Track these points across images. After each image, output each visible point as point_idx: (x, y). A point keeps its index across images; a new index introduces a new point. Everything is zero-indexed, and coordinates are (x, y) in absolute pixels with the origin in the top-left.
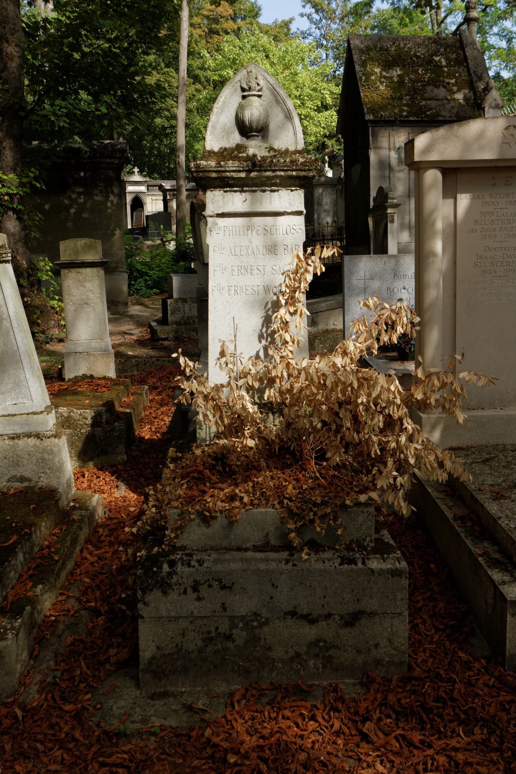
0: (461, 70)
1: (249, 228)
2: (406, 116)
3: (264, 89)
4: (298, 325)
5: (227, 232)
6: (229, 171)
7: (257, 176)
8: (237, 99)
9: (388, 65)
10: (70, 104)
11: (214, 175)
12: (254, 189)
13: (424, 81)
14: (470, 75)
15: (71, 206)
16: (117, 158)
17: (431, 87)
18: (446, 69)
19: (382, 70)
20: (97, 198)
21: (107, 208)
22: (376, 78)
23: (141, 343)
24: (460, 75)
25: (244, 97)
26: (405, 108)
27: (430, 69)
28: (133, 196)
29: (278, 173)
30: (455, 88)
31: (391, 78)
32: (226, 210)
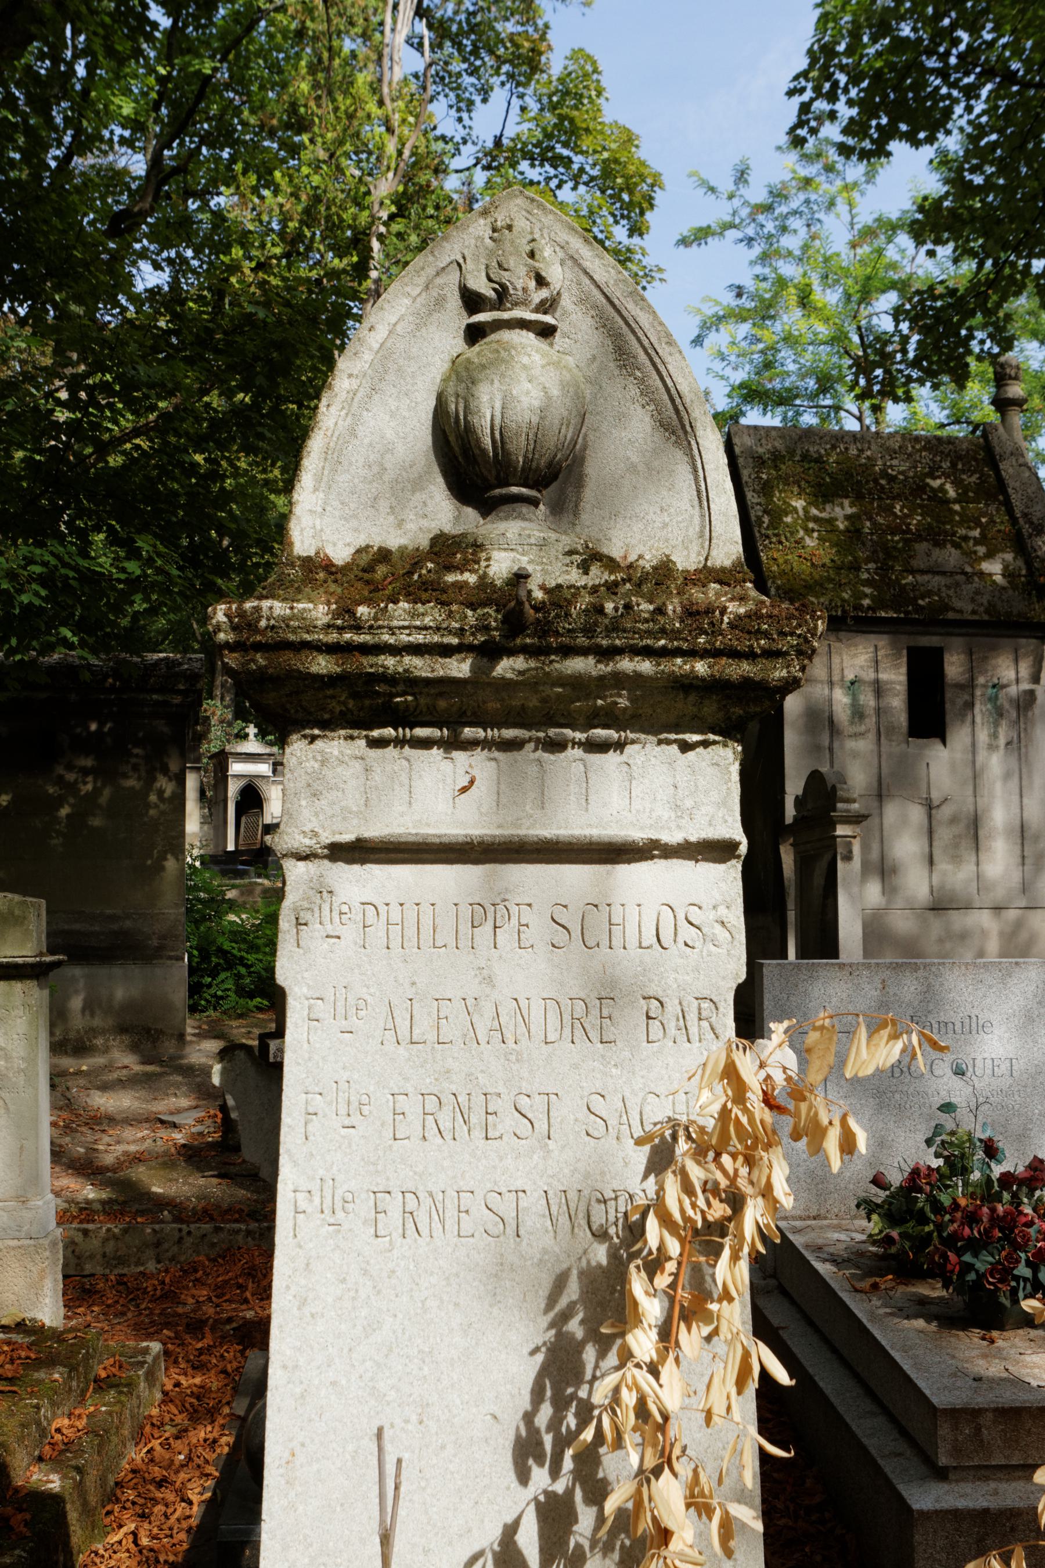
0: (992, 509)
1: (486, 913)
2: (869, 608)
3: (566, 302)
4: (719, 1409)
5: (377, 933)
6: (395, 650)
7: (530, 674)
8: (445, 340)
9: (824, 493)
10: (52, 554)
11: (322, 665)
12: (509, 733)
13: (908, 531)
14: (1013, 520)
15: (60, 802)
16: (179, 692)
17: (924, 546)
18: (957, 507)
19: (809, 504)
20: (131, 782)
21: (148, 806)
22: (795, 521)
23: (193, 1155)
24: (992, 521)
25: (474, 334)
26: (868, 590)
27: (921, 506)
28: (242, 783)
29: (626, 665)
30: (981, 550)
31: (831, 521)
32: (375, 830)
